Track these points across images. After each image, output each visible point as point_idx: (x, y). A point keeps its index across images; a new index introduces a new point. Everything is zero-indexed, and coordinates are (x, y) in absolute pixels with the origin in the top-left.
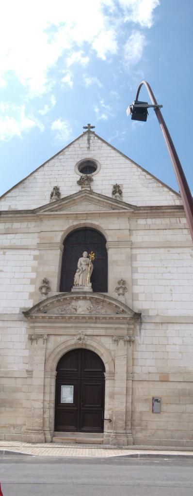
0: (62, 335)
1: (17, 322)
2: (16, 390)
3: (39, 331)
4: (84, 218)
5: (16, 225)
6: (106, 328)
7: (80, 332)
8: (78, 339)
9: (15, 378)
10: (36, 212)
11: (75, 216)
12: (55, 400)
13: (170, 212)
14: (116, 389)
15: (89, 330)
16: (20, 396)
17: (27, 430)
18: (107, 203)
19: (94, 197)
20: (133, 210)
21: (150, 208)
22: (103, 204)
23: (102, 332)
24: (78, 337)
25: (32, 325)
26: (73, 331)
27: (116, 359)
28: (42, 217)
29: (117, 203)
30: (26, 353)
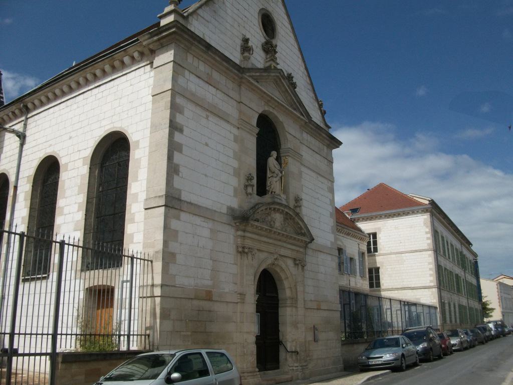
3: (248, 243)
4: (273, 106)
8: (275, 259)
9: (227, 302)
11: (270, 99)
12: (279, 351)
18: (292, 98)
19: (285, 84)
20: (307, 121)
21: (316, 126)
23: (288, 253)
29: (300, 105)
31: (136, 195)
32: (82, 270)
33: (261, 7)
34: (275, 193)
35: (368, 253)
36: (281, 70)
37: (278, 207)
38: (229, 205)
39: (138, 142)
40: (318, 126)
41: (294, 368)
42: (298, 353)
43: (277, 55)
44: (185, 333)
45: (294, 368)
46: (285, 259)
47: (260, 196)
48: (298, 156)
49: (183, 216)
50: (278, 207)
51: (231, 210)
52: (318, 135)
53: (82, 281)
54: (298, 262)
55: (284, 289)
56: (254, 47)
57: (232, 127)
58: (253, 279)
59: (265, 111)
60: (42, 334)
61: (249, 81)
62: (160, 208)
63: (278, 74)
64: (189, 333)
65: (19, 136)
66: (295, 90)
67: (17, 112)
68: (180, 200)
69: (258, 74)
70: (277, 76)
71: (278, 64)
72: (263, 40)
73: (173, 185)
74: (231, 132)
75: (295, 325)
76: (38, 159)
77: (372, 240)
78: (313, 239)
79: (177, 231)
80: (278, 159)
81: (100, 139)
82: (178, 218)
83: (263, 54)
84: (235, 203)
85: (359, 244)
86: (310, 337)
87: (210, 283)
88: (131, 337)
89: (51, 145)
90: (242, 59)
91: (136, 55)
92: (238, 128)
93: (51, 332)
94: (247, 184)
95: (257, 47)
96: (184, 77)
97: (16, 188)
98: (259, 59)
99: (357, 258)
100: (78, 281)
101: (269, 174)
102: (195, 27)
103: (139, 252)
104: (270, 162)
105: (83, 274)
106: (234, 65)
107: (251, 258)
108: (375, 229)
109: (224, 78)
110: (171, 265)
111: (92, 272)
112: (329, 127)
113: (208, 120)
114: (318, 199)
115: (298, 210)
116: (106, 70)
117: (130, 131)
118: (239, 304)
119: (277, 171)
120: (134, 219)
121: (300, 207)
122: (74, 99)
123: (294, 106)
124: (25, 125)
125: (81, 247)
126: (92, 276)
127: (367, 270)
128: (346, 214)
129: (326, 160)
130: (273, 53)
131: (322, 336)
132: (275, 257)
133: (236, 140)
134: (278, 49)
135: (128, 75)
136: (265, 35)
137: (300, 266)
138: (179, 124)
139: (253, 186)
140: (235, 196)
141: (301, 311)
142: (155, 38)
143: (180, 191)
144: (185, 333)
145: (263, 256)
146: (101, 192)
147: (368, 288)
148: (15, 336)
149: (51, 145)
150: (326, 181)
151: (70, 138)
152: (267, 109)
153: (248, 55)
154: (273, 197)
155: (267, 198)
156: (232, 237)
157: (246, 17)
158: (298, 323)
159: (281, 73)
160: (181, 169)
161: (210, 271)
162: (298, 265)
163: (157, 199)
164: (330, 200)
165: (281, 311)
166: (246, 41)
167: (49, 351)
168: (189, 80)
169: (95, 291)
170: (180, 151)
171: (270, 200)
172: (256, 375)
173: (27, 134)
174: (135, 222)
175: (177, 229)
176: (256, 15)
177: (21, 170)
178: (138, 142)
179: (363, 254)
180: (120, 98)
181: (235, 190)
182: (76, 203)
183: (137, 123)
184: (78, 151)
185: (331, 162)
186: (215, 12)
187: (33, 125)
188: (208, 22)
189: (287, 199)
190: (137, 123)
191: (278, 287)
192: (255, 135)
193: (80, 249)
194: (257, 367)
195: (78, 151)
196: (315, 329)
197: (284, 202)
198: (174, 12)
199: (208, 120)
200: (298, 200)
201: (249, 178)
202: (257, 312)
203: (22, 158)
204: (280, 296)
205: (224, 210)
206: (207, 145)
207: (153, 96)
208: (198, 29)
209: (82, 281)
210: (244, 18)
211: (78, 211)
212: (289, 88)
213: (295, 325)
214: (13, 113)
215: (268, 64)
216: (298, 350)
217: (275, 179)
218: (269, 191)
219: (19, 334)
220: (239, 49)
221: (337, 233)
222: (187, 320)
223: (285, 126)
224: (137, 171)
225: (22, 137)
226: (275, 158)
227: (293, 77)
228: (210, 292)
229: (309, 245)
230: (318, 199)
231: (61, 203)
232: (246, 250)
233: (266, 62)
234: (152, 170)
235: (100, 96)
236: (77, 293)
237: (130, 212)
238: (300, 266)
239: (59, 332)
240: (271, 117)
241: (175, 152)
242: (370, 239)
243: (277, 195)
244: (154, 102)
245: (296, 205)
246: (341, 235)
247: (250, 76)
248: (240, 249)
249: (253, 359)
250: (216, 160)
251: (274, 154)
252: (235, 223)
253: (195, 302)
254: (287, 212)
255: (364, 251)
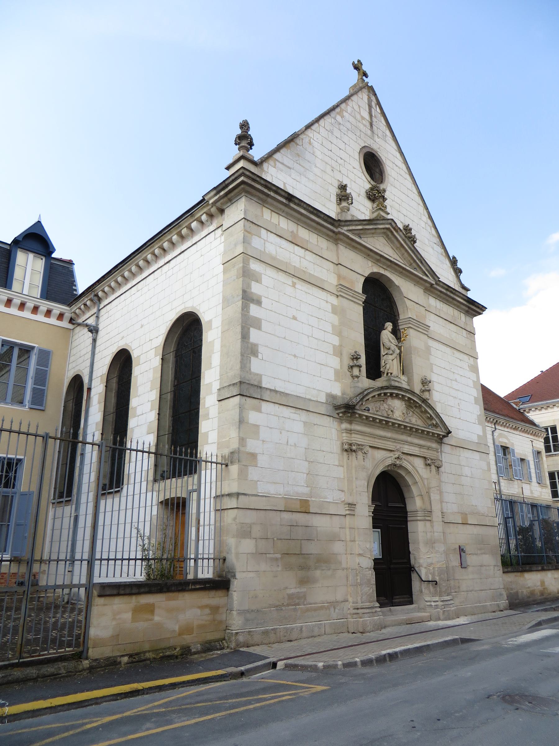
0: (378, 448)
1: (325, 417)
2: (333, 538)
3: (357, 439)
5: (304, 234)
6: (421, 446)
7: (398, 446)
10: (339, 226)
13: (441, 292)
14: (436, 534)
15: (406, 446)
16: (338, 547)
17: (354, 609)
22: (403, 254)
23: (415, 450)
24: (397, 454)
25: (345, 425)
26: (390, 445)
27: (431, 491)
28: (341, 237)
30: (340, 472)
31: (210, 384)
32: (155, 480)
33: (363, 145)
34: (391, 374)
35: (546, 452)
36: (392, 220)
37: (396, 392)
38: (329, 391)
39: (210, 322)
40: (448, 288)
41: (433, 604)
42: (436, 584)
43: (387, 203)
44: (271, 556)
45: (433, 604)
46: (411, 458)
47: (374, 379)
48: (423, 328)
49: (265, 406)
50: (396, 392)
51: (331, 397)
52: (451, 300)
53: (155, 493)
54: (429, 462)
55: (413, 497)
56: (354, 195)
57: (329, 295)
58: (366, 484)
59: (373, 273)
60: (108, 560)
61: (348, 237)
62: (235, 398)
63: (388, 226)
64: (279, 556)
65: (91, 331)
66: (415, 245)
67: (88, 303)
68: (261, 387)
69: (360, 227)
70: (388, 229)
71: (388, 214)
72: (368, 186)
73: (250, 370)
74: (327, 302)
75: (431, 543)
76: (111, 355)
77: (550, 435)
78: (450, 432)
79: (258, 426)
80: (395, 332)
81: (172, 323)
82: (259, 410)
83: (369, 204)
84: (337, 390)
85: (532, 441)
86: (455, 561)
87: (306, 490)
88: (200, 562)
89: (123, 338)
90: (339, 211)
91: (204, 218)
92: (337, 296)
93: (86, 556)
94: (351, 364)
95: (359, 195)
96: (260, 237)
97: (89, 389)
98: (363, 209)
99: (530, 458)
100: (149, 494)
101: (383, 352)
102: (272, 176)
103: (214, 454)
104: (384, 337)
105: (156, 485)
106: (327, 218)
107: (362, 458)
108: (554, 420)
109: (316, 236)
110: (250, 468)
111: (168, 481)
112: (467, 290)
113: (295, 288)
114: (456, 381)
115: (426, 395)
116: (174, 241)
117: (201, 311)
118: (348, 517)
119: (393, 347)
120: (208, 414)
121: (429, 391)
122: (145, 280)
123: (414, 265)
124: (98, 317)
125: (152, 453)
126: (168, 487)
127: (547, 475)
128: (512, 404)
129: (464, 331)
130: (381, 200)
131: (471, 560)
132: (397, 456)
133: (335, 310)
134: (387, 195)
135: (198, 243)
136: (369, 179)
137: (433, 467)
138: (255, 294)
139: (360, 366)
140: (337, 380)
141: (438, 527)
142: (222, 193)
143: (260, 376)
144: (271, 556)
145: (380, 455)
146: (176, 385)
147: (551, 498)
148: (76, 562)
149: (123, 338)
150: (465, 357)
151: (142, 326)
152: (375, 270)
153: (347, 205)
154: (389, 380)
155: (380, 382)
156: (334, 432)
157: (341, 159)
158: (434, 543)
159: (393, 224)
160: (261, 349)
161: (305, 475)
162: (429, 465)
163: (231, 388)
164: (473, 381)
165: (411, 526)
166: (343, 188)
167: (84, 581)
168: (267, 241)
169: (173, 504)
170: (259, 327)
171: (385, 384)
172: (376, 612)
173: (101, 327)
174: (209, 419)
175: (257, 424)
176: (357, 156)
177: (95, 369)
178: (210, 322)
179: (539, 453)
180: (191, 273)
181: (337, 372)
182: (149, 401)
183: (209, 299)
184: (150, 340)
185: (472, 333)
186: (299, 156)
187: (105, 317)
188: (290, 168)
189: (409, 382)
190: (209, 299)
191: (406, 495)
192: (362, 303)
193: (152, 456)
194: (378, 601)
195: (150, 340)
196: (461, 550)
197: (405, 386)
198: (243, 159)
199: (295, 288)
200: (425, 382)
201: (356, 358)
202: (374, 527)
203: (96, 356)
204: (409, 508)
205: (323, 399)
206: (295, 318)
207: (223, 264)
208: (276, 178)
209: (155, 493)
210: (340, 161)
211: (151, 411)
212: (405, 242)
213: (431, 543)
214: (85, 305)
215: (375, 215)
216: (437, 579)
217: (391, 357)
218: (384, 373)
219: (101, 560)
220: (334, 198)
221: (487, 424)
222: (275, 539)
223: (403, 289)
224: (211, 357)
225: (94, 330)
226: (391, 330)
227: (411, 229)
228: (307, 501)
229: (446, 440)
230: (456, 381)
231: (134, 402)
232: (354, 448)
233: (373, 213)
234: (225, 354)
235: (169, 273)
236: (148, 509)
237: (205, 405)
238: (433, 467)
239: (98, 556)
240: (383, 281)
241: (251, 329)
242: (548, 434)
243: (395, 377)
244: (225, 271)
245: (423, 389)
246: (506, 429)
247: (349, 231)
248: (346, 447)
249: (371, 589)
250: (308, 336)
251: (389, 326)
252: (338, 414)
253: (286, 516)
254: (409, 398)
255: (540, 450)
